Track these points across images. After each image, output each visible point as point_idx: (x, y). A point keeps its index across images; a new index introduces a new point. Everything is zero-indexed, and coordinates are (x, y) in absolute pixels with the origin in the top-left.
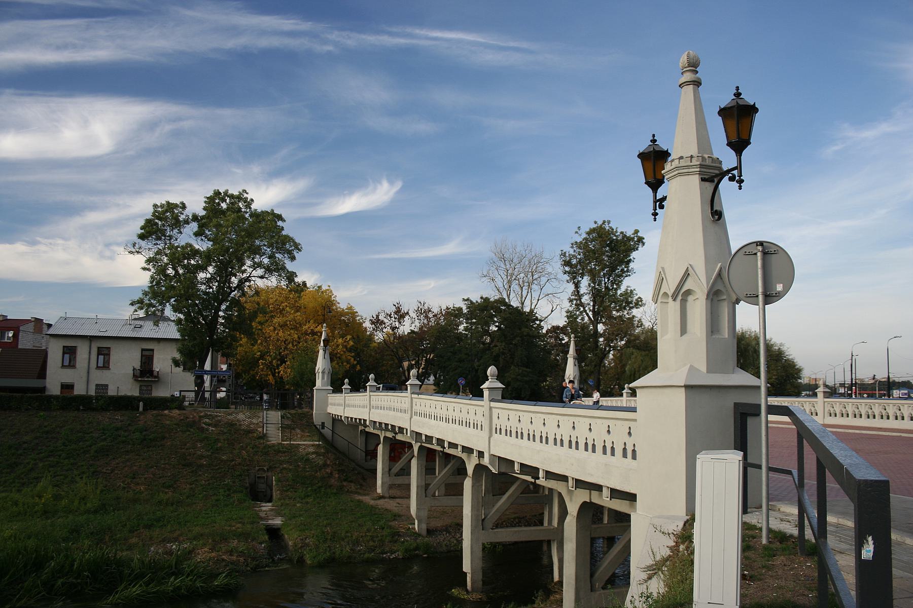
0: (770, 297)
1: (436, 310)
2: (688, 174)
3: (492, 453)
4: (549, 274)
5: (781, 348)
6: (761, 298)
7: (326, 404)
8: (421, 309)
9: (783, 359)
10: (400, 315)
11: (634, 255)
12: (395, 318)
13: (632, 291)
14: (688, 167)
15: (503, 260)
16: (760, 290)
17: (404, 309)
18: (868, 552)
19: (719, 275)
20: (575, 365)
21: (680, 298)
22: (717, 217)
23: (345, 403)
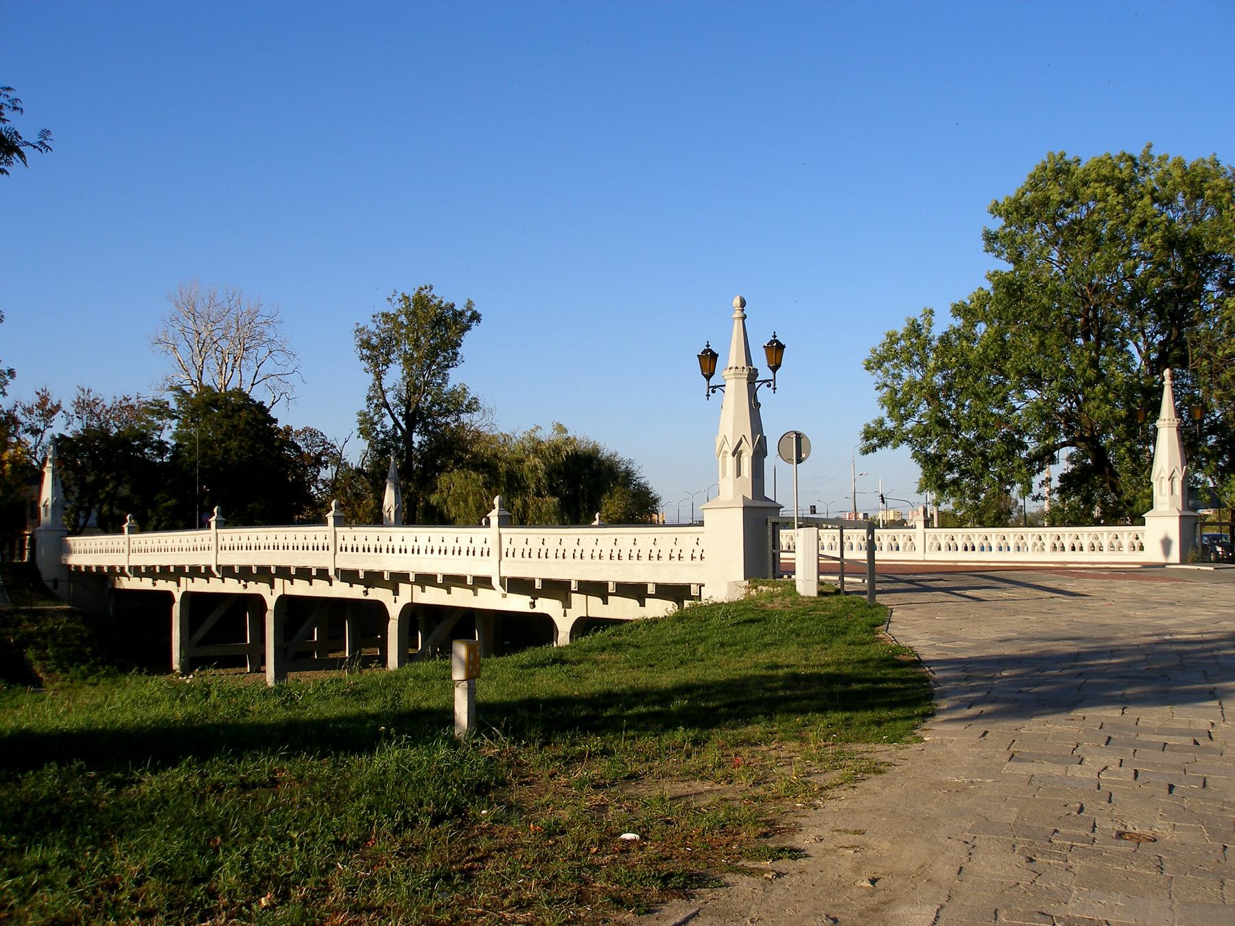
0: (799, 460)
2: (741, 378)
5: (630, 466)
8: (84, 401)
9: (631, 483)
11: (467, 338)
14: (741, 374)
15: (190, 315)
18: (870, 538)
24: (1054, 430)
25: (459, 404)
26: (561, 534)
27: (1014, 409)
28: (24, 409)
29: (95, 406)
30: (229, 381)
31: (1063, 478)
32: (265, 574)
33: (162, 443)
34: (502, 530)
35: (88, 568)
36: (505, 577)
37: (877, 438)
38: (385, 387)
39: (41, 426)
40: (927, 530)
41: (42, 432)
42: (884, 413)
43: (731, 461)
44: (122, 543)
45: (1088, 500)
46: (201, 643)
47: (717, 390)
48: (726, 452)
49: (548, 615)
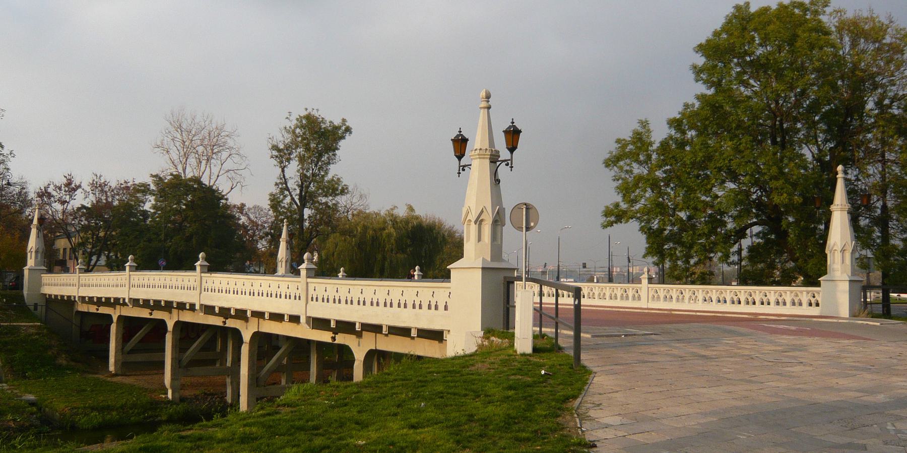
1: (113, 184)
2: (484, 158)
3: (308, 315)
4: (230, 148)
6: (524, 229)
7: (40, 284)
8: (97, 182)
10: (71, 187)
11: (342, 143)
12: (65, 191)
13: (339, 179)
14: (484, 155)
15: (179, 130)
16: (524, 225)
17: (76, 181)
18: (576, 303)
19: (498, 212)
20: (288, 249)
21: (478, 223)
22: (497, 182)
23: (79, 283)
24: (748, 212)
25: (336, 189)
26: (349, 285)
27: (717, 197)
28: (56, 186)
29: (104, 186)
30: (203, 173)
31: (751, 249)
32: (168, 306)
33: (145, 212)
34: (309, 280)
35: (56, 296)
36: (310, 317)
37: (615, 216)
38: (287, 176)
39: (67, 198)
40: (650, 285)
41: (68, 203)
42: (619, 198)
43: (474, 228)
44: (124, 279)
45: (772, 266)
46: (132, 351)
47: (466, 168)
48: (470, 221)
49: (348, 346)
